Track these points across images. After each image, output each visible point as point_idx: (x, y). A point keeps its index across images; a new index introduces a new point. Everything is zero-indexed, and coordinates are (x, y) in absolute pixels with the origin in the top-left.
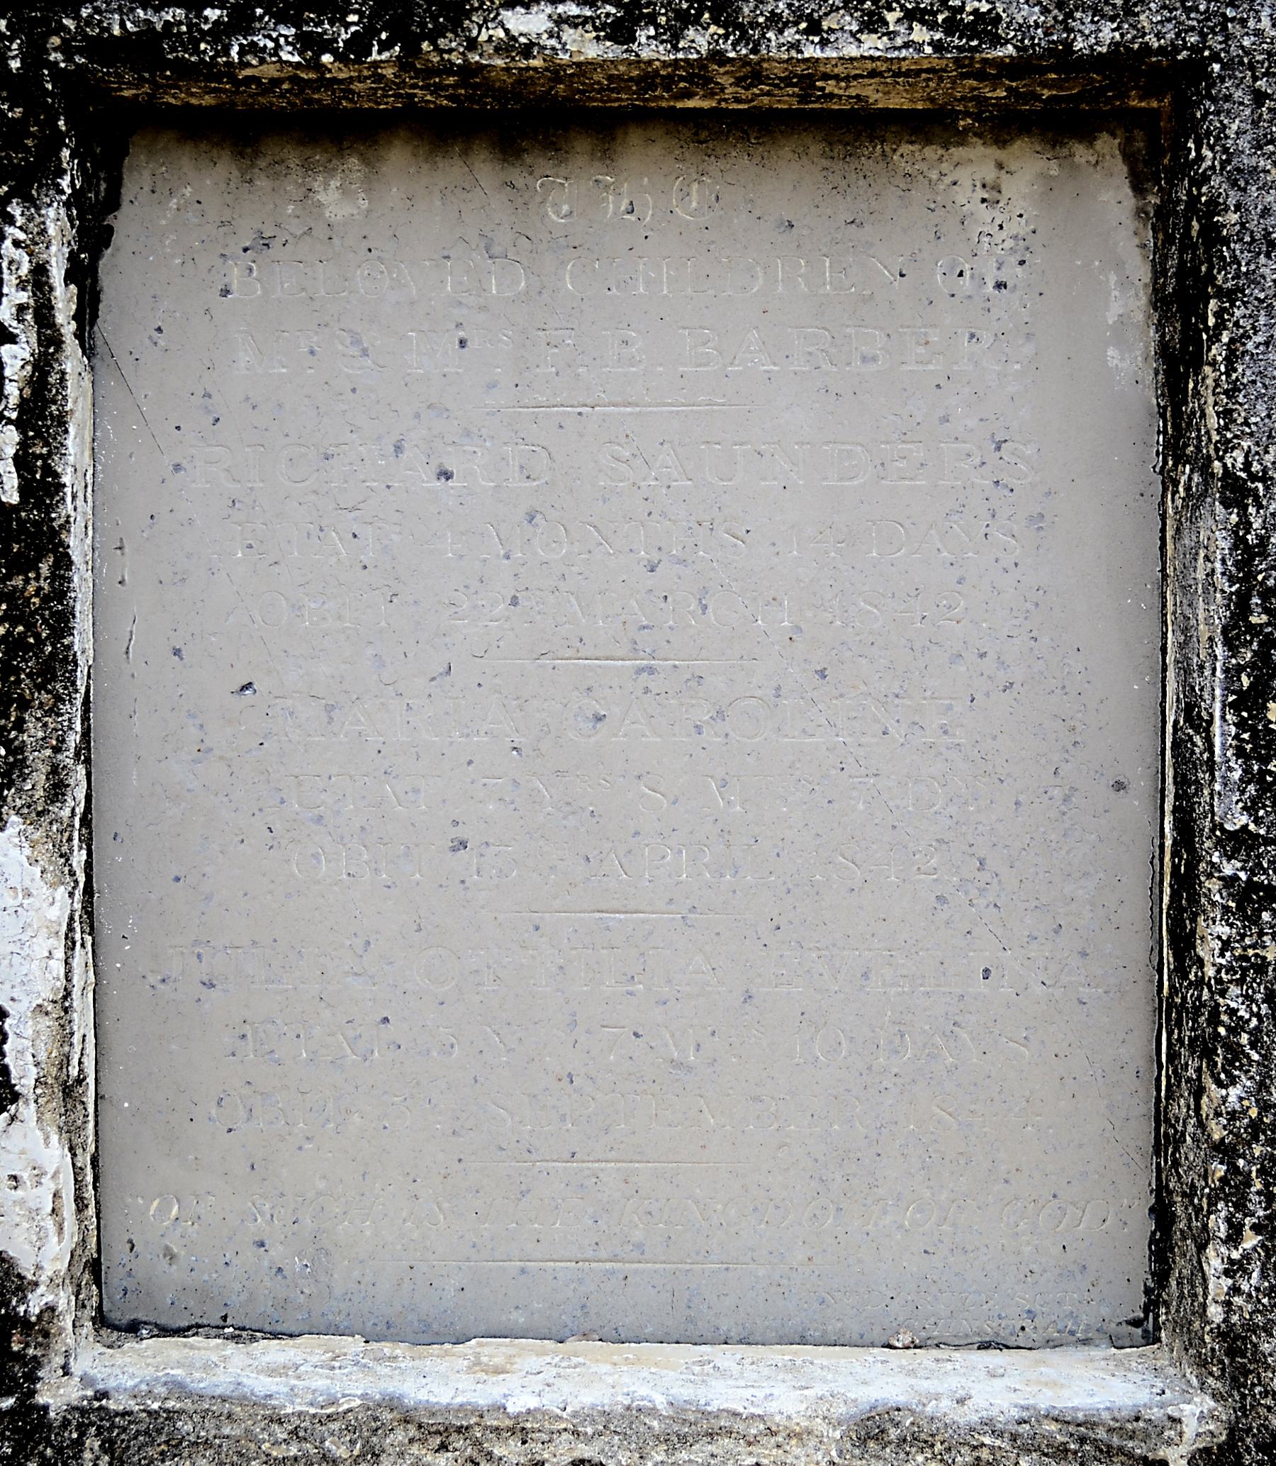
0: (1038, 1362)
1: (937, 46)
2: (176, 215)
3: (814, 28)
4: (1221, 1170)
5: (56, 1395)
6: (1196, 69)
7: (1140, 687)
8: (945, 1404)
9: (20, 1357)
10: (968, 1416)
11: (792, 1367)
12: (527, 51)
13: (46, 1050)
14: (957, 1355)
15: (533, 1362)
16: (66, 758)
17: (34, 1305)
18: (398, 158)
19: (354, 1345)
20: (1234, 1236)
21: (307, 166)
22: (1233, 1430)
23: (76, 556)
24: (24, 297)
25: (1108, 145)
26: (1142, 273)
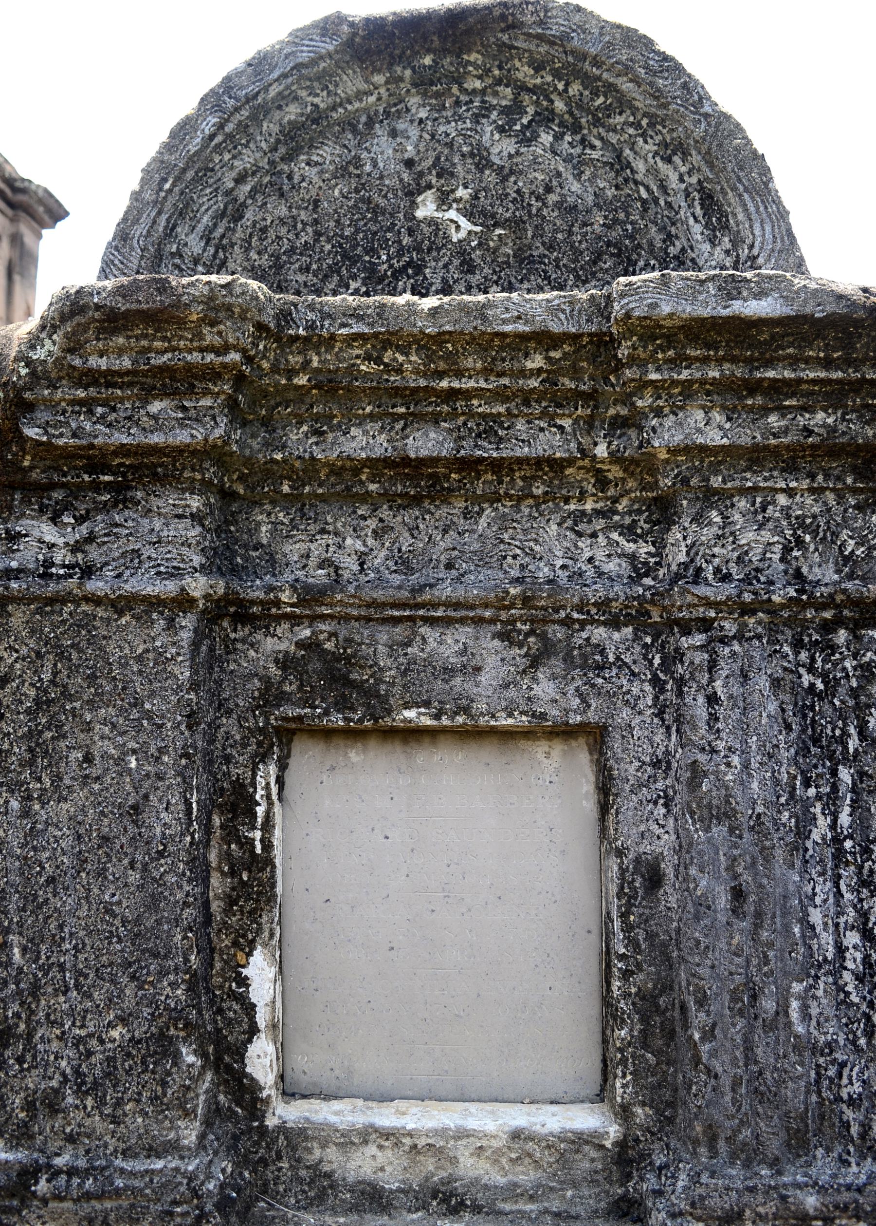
0: (568, 1110)
1: (529, 722)
2: (306, 758)
3: (493, 716)
4: (619, 1056)
5: (271, 1122)
6: (605, 727)
7: (593, 902)
8: (538, 1127)
9: (260, 1109)
10: (545, 1131)
11: (492, 1112)
12: (410, 721)
13: (268, 1017)
14: (543, 1107)
15: (414, 1110)
16: (274, 925)
17: (265, 1094)
18: (372, 743)
19: (360, 1102)
20: (624, 1076)
21: (346, 746)
22: (625, 1136)
23: (277, 864)
24: (263, 792)
25: (582, 741)
26: (592, 778)
